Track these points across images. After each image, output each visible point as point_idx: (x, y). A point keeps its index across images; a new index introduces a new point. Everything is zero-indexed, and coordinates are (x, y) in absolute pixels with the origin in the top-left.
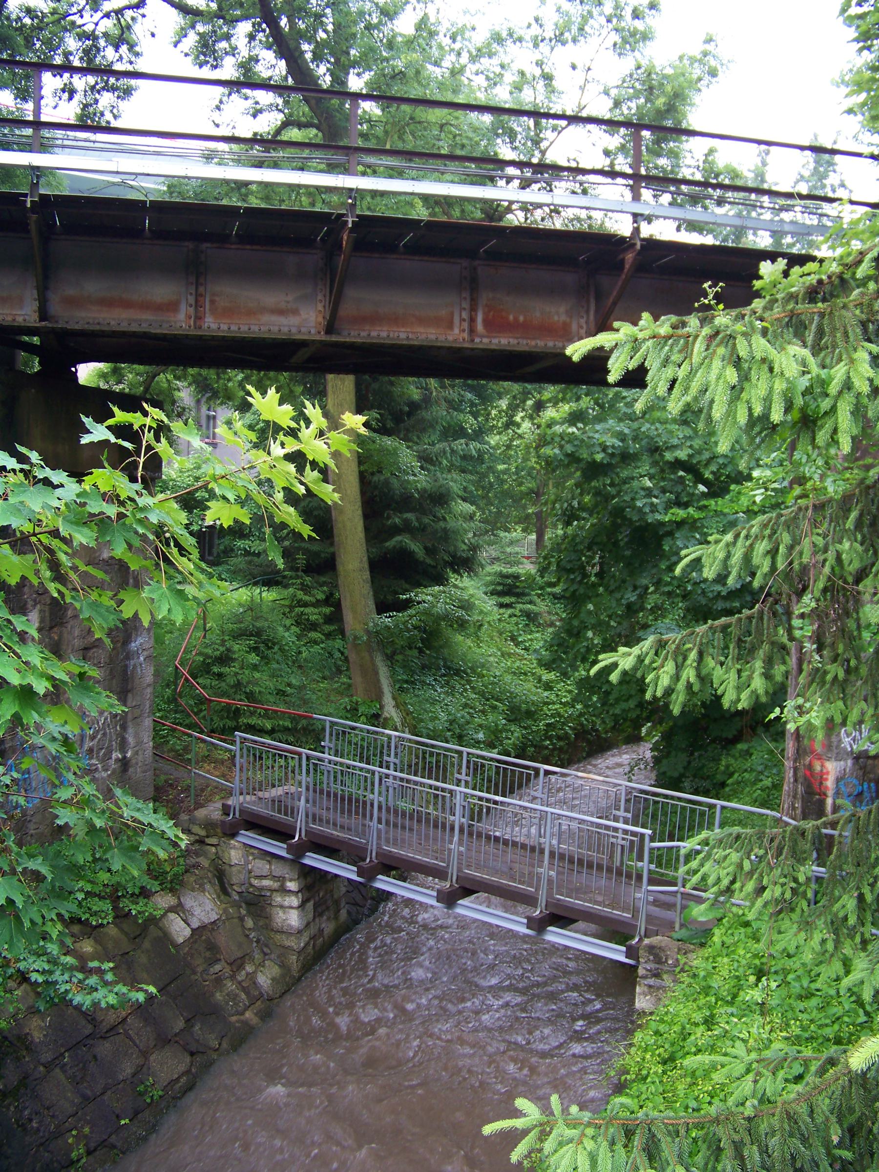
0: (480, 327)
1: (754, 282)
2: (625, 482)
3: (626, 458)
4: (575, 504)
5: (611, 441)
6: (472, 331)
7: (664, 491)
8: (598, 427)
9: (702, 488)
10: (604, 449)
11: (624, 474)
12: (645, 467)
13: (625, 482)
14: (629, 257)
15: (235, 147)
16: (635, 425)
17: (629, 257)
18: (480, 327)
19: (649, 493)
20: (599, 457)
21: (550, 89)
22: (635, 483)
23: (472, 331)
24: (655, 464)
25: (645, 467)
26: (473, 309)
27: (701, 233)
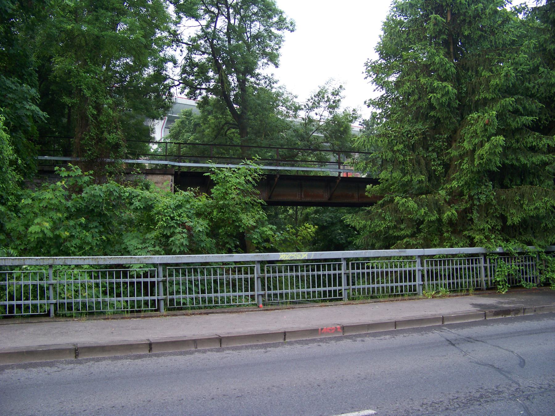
0: (303, 196)
1: (151, 145)
2: (333, 231)
3: (333, 224)
4: (316, 238)
5: (328, 219)
6: (301, 197)
7: (344, 234)
8: (324, 215)
9: (356, 232)
10: (326, 221)
11: (333, 229)
12: (339, 227)
13: (333, 231)
14: (338, 181)
15: (281, 199)
16: (335, 214)
17: (338, 181)
18: (303, 196)
19: (340, 234)
20: (325, 224)
21: (89, 183)
22: (336, 232)
23: (301, 197)
24: (341, 226)
25: (339, 227)
26: (301, 192)
27: (259, 165)
